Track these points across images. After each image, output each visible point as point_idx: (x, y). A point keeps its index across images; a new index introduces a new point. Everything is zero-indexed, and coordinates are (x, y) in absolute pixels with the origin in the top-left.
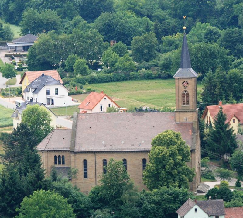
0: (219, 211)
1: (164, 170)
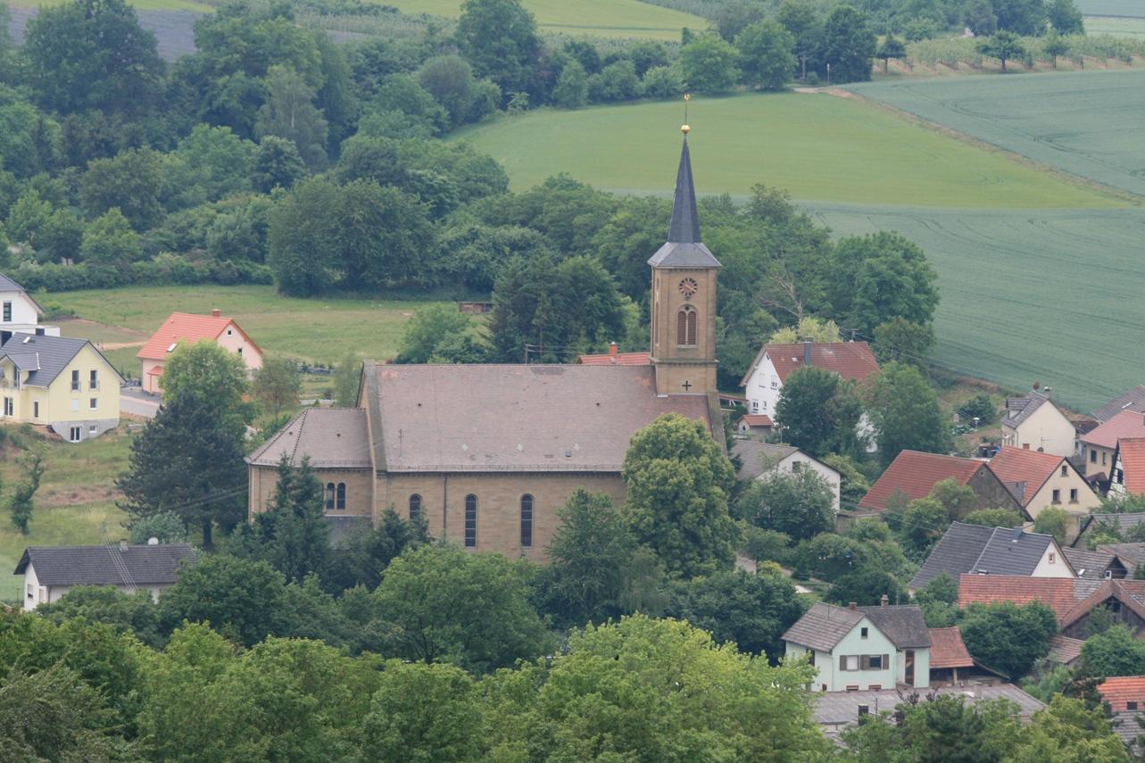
0: (914, 637)
1: (675, 524)
